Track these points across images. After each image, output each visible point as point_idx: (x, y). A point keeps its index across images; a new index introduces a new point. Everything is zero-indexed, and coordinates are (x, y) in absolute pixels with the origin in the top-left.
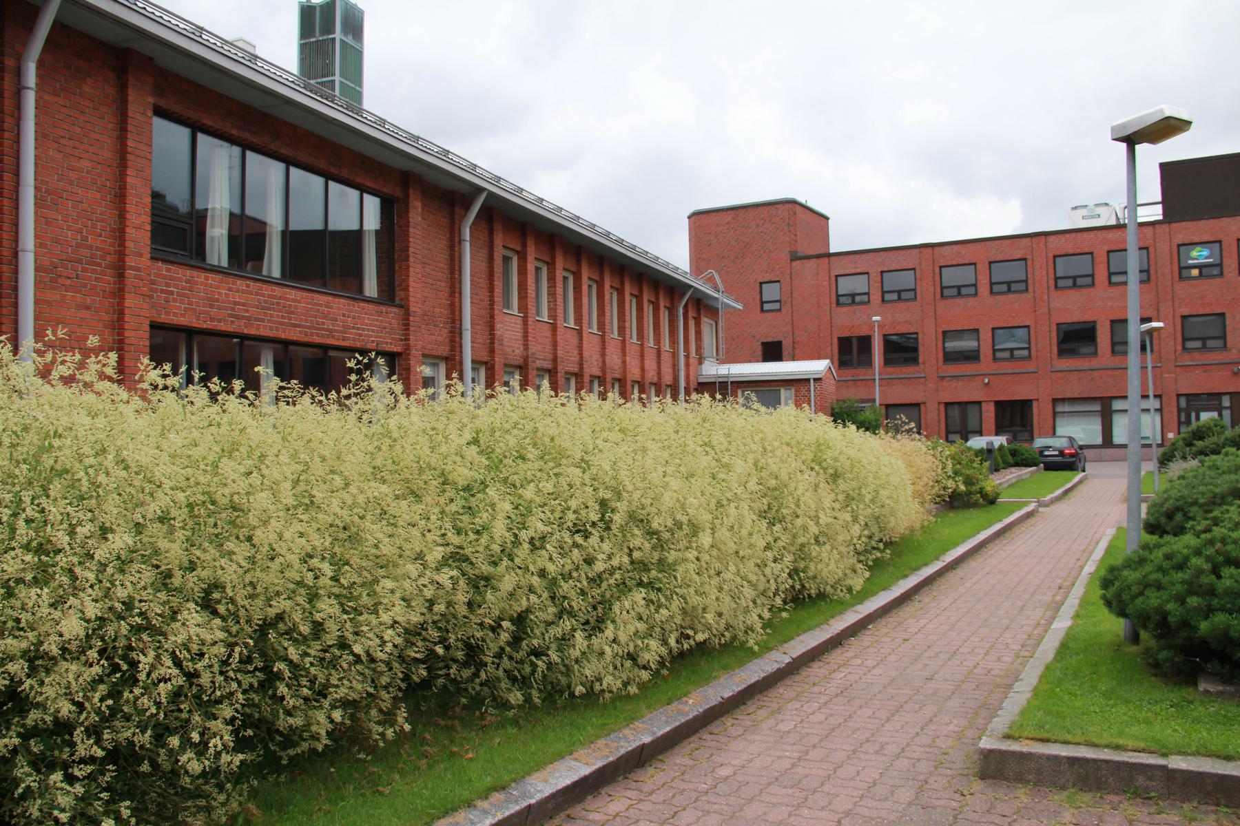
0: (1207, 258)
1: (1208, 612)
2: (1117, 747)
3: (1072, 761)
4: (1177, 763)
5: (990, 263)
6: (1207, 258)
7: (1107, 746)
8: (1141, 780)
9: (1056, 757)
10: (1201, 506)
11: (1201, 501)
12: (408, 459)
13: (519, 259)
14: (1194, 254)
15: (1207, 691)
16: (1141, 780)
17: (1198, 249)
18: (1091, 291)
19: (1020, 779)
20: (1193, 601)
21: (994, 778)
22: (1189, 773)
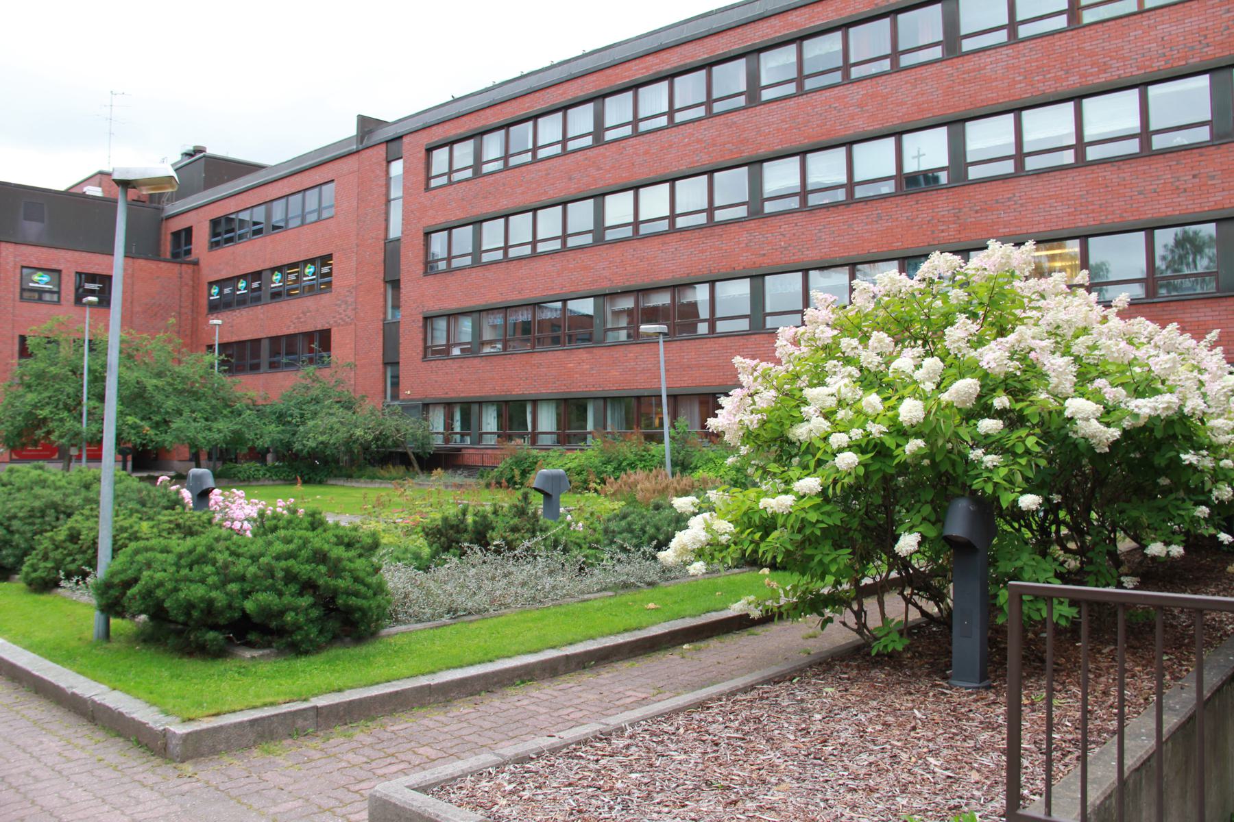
0: (47, 283)
1: (246, 594)
2: (272, 704)
3: (253, 722)
4: (321, 701)
5: (426, 319)
6: (47, 283)
7: (265, 705)
8: (300, 723)
9: (241, 723)
10: (21, 519)
11: (21, 515)
12: (599, 442)
13: (393, 288)
14: (36, 278)
15: (253, 657)
16: (300, 723)
17: (40, 273)
18: (55, 309)
19: (214, 751)
20: (233, 587)
21: (192, 758)
22: (330, 706)
